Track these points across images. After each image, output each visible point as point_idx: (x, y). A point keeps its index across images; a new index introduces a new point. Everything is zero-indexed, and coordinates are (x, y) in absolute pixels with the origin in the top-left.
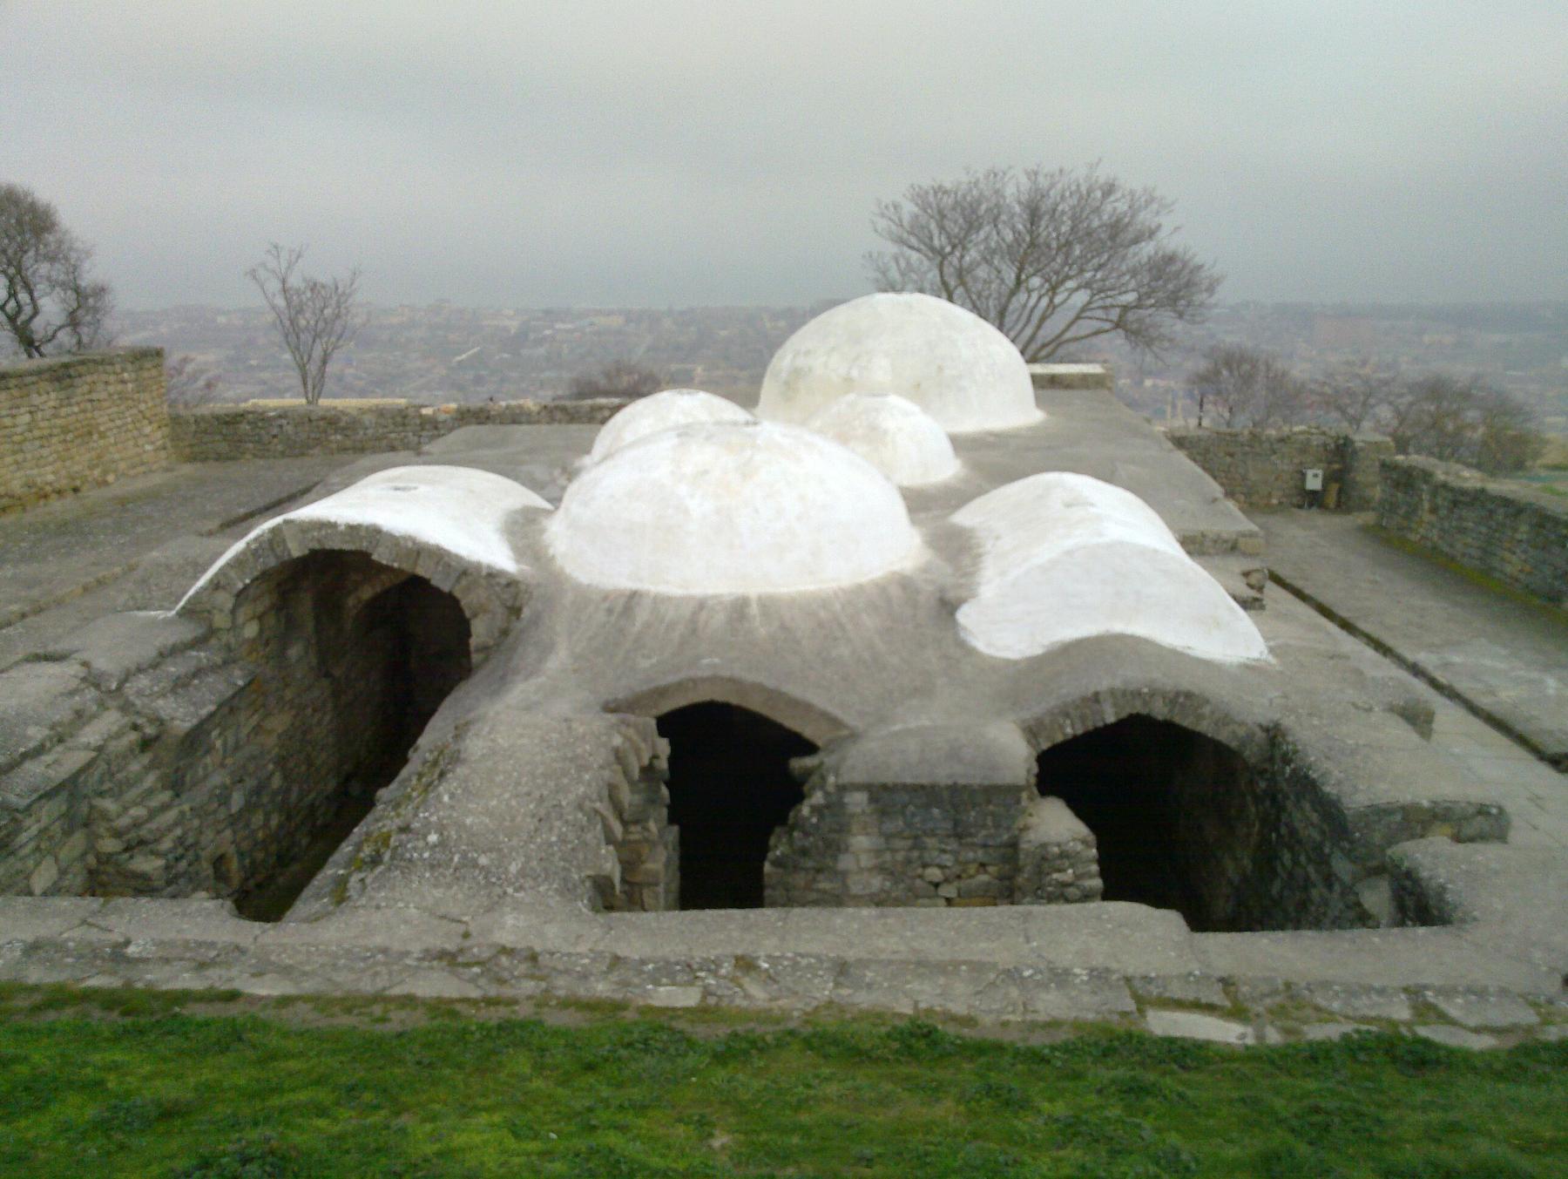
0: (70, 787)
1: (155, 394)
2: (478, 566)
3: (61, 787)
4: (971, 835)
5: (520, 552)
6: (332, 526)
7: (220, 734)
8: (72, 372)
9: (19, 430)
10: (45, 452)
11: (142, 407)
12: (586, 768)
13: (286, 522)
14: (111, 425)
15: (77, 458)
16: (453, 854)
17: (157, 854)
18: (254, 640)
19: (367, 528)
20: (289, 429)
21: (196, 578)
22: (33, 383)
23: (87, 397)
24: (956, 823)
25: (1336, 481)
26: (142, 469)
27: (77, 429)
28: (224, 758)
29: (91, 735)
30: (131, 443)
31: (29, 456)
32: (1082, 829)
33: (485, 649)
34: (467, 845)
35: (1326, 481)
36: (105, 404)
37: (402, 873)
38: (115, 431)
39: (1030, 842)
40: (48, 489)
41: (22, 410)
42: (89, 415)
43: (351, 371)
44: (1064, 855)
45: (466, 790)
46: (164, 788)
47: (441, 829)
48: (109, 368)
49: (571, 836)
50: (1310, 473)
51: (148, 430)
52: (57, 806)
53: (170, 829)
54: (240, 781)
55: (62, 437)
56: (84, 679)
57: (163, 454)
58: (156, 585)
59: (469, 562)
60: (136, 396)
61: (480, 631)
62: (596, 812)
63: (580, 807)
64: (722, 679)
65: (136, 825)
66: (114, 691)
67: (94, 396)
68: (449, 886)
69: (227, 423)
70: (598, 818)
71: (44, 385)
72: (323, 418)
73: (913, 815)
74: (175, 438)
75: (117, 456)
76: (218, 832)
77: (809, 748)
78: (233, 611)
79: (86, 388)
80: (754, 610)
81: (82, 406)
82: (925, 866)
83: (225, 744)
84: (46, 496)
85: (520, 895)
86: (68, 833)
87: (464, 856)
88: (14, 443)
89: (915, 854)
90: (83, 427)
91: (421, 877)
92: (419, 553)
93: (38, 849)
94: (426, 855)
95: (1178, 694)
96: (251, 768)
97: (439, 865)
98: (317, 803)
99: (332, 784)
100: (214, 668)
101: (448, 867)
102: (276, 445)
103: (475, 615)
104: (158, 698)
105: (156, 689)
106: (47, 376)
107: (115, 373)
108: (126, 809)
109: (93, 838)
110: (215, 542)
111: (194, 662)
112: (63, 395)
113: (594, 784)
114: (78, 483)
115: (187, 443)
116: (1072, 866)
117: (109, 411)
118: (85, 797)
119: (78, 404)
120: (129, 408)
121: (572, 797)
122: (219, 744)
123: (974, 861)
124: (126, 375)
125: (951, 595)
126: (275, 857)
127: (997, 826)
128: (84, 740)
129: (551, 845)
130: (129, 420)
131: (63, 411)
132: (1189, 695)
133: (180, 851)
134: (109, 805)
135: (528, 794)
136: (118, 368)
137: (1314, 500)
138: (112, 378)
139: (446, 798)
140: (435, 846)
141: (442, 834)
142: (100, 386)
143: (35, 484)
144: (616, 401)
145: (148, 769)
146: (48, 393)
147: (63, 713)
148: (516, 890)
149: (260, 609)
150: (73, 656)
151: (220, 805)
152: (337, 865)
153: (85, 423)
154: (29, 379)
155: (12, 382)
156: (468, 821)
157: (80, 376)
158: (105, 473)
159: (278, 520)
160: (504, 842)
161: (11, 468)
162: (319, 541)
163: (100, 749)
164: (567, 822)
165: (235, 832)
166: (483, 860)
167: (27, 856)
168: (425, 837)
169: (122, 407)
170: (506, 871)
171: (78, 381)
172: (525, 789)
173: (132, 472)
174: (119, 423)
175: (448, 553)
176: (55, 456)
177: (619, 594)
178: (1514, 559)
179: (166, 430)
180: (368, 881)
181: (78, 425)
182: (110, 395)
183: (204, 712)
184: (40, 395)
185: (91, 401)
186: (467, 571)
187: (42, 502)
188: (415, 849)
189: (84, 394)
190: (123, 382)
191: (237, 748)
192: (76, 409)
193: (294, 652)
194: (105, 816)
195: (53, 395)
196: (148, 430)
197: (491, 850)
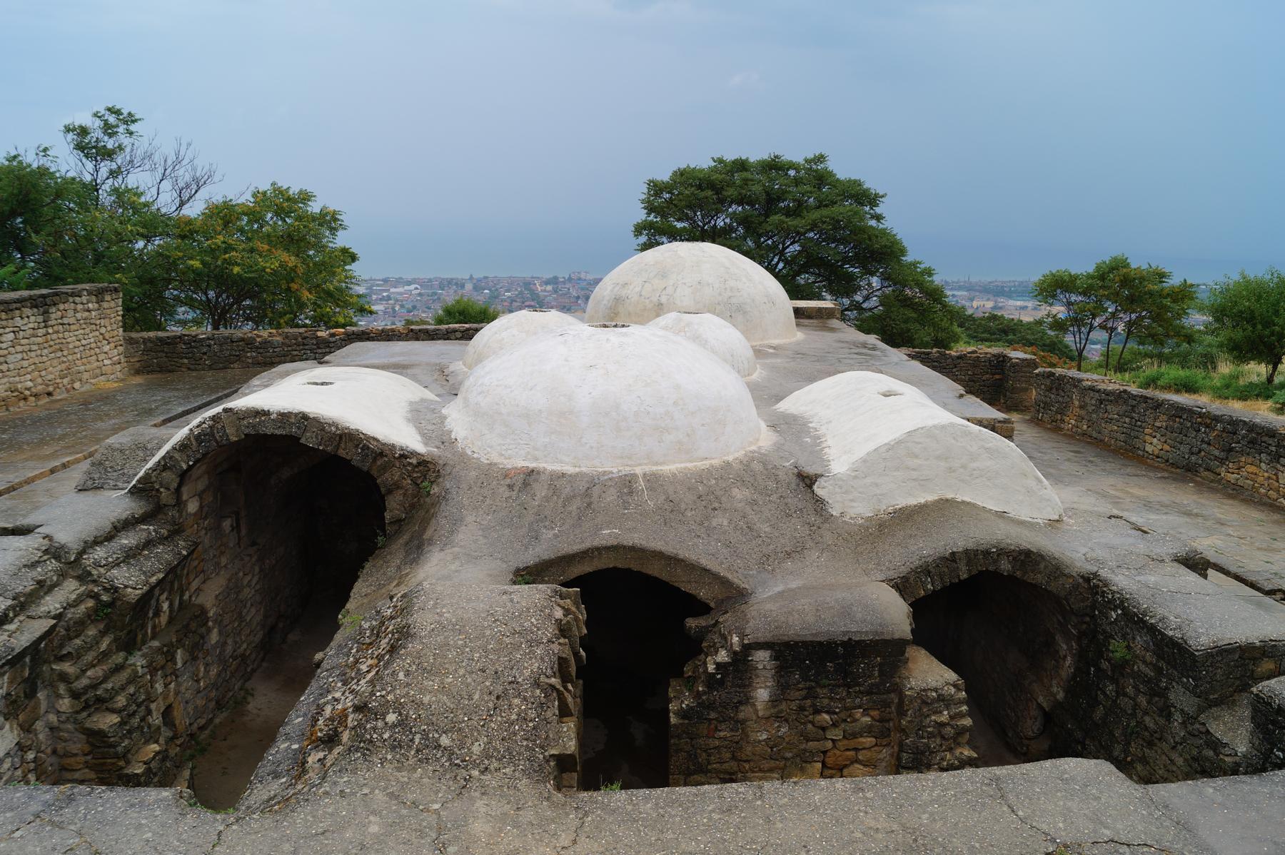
5: (426, 439)
6: (266, 413)
10: (25, 363)
11: (103, 330)
13: (225, 410)
15: (51, 368)
17: (113, 711)
18: (195, 514)
19: (296, 415)
21: (145, 461)
23: (60, 321)
27: (51, 346)
29: (52, 603)
31: (12, 366)
32: (951, 676)
33: (399, 521)
34: (428, 725)
36: (73, 327)
37: (364, 755)
38: (82, 348)
39: (911, 689)
40: (27, 393)
41: (7, 330)
42: (61, 335)
44: (941, 698)
46: (119, 650)
47: (398, 708)
48: (77, 299)
49: (532, 713)
51: (106, 348)
53: (123, 688)
55: (39, 352)
56: (46, 552)
58: (111, 467)
59: (384, 444)
60: (98, 322)
61: (394, 506)
62: (553, 687)
63: (537, 684)
64: (624, 547)
65: (94, 686)
66: (72, 562)
71: (27, 311)
75: (82, 368)
77: (702, 608)
82: (817, 711)
85: (487, 777)
87: (425, 735)
89: (808, 702)
90: (55, 344)
91: (383, 761)
92: (341, 436)
94: (386, 736)
97: (401, 747)
98: (248, 652)
99: (260, 635)
100: (163, 540)
102: (205, 360)
103: (390, 492)
104: (113, 567)
105: (110, 560)
107: (82, 304)
108: (84, 671)
110: (163, 431)
111: (144, 535)
113: (546, 659)
114: (51, 389)
115: (136, 359)
116: (947, 707)
117: (76, 333)
120: (92, 331)
121: (527, 673)
125: (810, 470)
126: (214, 703)
128: (43, 609)
130: (92, 340)
132: (1028, 553)
133: (134, 707)
134: (67, 667)
136: (84, 299)
138: (80, 307)
140: (394, 726)
141: (400, 714)
142: (71, 313)
143: (16, 390)
144: (475, 326)
145: (103, 634)
146: (28, 317)
147: (25, 584)
148: (482, 773)
150: (36, 531)
151: (167, 661)
152: (288, 737)
153: (58, 341)
154: (14, 306)
156: (426, 700)
157: (55, 304)
158: (73, 381)
159: (218, 409)
160: (464, 721)
162: (254, 426)
163: (59, 617)
164: (525, 699)
166: (445, 741)
168: (384, 715)
169: (87, 331)
170: (470, 753)
174: (84, 342)
176: (33, 367)
177: (518, 471)
178: (1155, 441)
179: (121, 349)
180: (328, 763)
181: (52, 343)
183: (153, 580)
184: (22, 318)
188: (374, 729)
189: (56, 319)
190: (89, 311)
195: (32, 319)
196: (106, 348)
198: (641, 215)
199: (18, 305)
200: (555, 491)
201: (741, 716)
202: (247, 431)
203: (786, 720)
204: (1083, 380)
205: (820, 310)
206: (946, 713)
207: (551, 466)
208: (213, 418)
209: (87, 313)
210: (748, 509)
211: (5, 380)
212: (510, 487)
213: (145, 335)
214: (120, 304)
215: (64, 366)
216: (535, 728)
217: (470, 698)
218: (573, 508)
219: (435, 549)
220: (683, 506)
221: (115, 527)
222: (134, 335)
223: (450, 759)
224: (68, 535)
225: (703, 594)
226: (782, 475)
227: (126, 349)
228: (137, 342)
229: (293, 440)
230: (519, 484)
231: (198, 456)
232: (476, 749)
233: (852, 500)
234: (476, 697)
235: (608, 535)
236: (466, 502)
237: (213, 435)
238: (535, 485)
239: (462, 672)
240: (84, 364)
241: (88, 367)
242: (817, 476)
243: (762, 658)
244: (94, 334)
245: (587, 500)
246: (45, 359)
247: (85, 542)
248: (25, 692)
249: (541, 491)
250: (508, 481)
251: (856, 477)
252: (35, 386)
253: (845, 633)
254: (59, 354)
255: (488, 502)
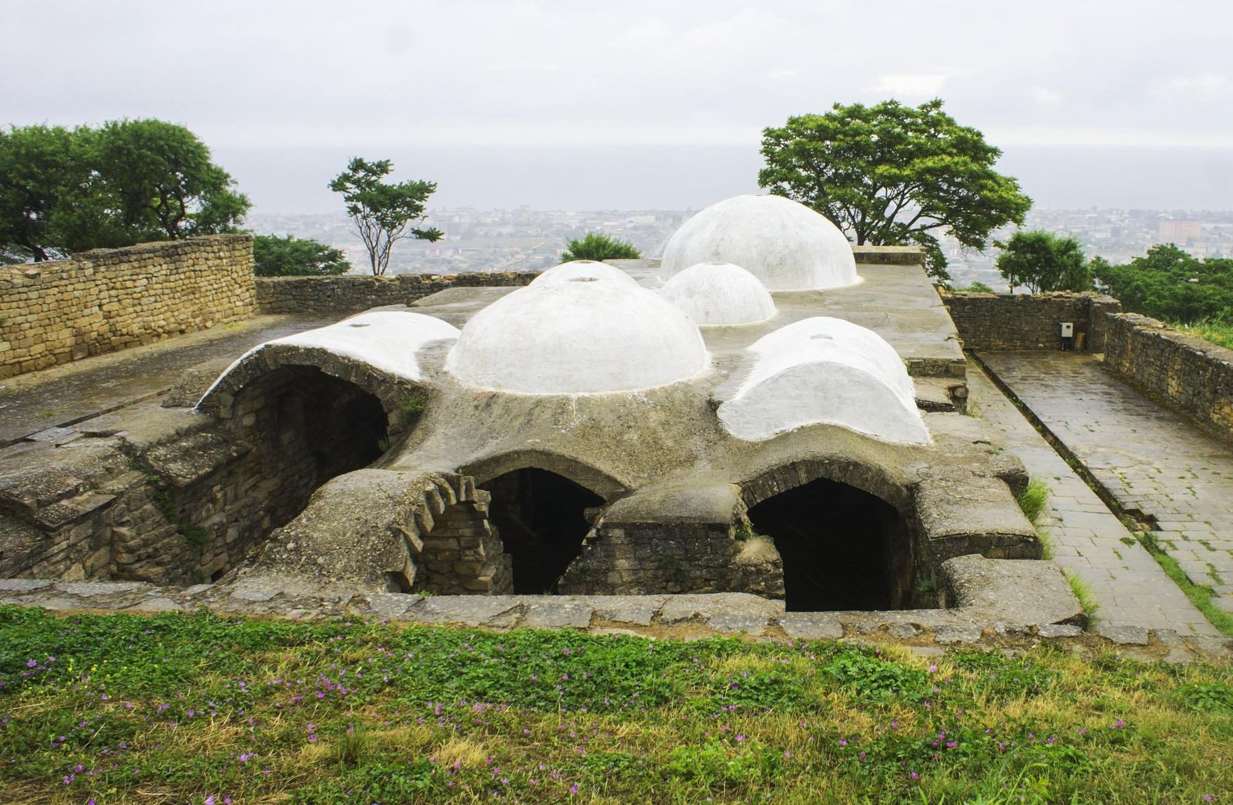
0: (96, 516)
1: (244, 267)
2: (392, 377)
3: (86, 516)
4: (698, 560)
5: (424, 368)
6: (296, 349)
7: (221, 490)
8: (180, 251)
9: (137, 290)
10: (158, 305)
11: (235, 275)
12: (400, 503)
14: (210, 287)
16: (302, 556)
18: (251, 427)
19: (318, 350)
20: (339, 291)
22: (149, 258)
24: (687, 551)
25: (1083, 331)
26: (233, 318)
27: (183, 290)
28: (225, 505)
30: (226, 300)
31: (145, 308)
35: (1075, 331)
36: (204, 274)
38: (213, 292)
40: (160, 330)
41: (141, 276)
42: (193, 281)
43: (458, 257)
44: (759, 572)
45: (318, 516)
48: (209, 249)
49: (380, 546)
50: (1064, 325)
51: (238, 291)
52: (87, 529)
54: (236, 521)
55: (171, 295)
56: (120, 449)
57: (250, 308)
60: (229, 268)
64: (536, 452)
67: (197, 268)
68: (296, 576)
69: (295, 287)
70: (402, 536)
72: (363, 284)
73: (657, 545)
74: (259, 297)
75: (214, 309)
76: (216, 555)
78: (233, 406)
79: (191, 262)
80: (573, 406)
81: (188, 274)
83: (225, 495)
84: (159, 336)
86: (94, 548)
87: (309, 558)
88: (134, 299)
93: (67, 558)
95: (849, 464)
96: (245, 512)
97: (292, 563)
100: (218, 444)
101: (298, 564)
103: (391, 411)
106: (160, 253)
107: (214, 252)
109: (114, 552)
112: (172, 266)
114: (183, 327)
118: (109, 525)
119: (184, 273)
121: (386, 521)
122: (219, 495)
123: (701, 577)
124: (222, 254)
125: (716, 398)
127: (714, 552)
129: (366, 552)
130: (224, 284)
131: (172, 278)
135: (358, 519)
136: (216, 249)
137: (1067, 346)
138: (211, 255)
139: (304, 521)
140: (291, 550)
142: (202, 261)
143: (150, 328)
146: (160, 265)
148: (338, 580)
149: (257, 405)
154: (147, 256)
155: (133, 257)
156: (315, 535)
158: (205, 321)
161: (132, 316)
164: (379, 537)
165: (230, 556)
166: (321, 560)
167: (58, 562)
169: (219, 276)
170: (334, 568)
171: (184, 257)
172: (357, 516)
173: (225, 320)
174: (215, 286)
175: (372, 368)
179: (253, 292)
181: (184, 287)
182: (209, 267)
185: (194, 271)
186: (387, 380)
187: (155, 339)
188: (278, 552)
190: (220, 258)
191: (236, 498)
192: (182, 276)
193: (286, 437)
194: (122, 538)
195: (165, 266)
196: (238, 291)
197: (326, 554)
198: (763, 163)
199: (151, 255)
200: (507, 411)
201: (610, 580)
202: (282, 362)
203: (645, 585)
204: (1135, 325)
205: (905, 255)
206: (763, 584)
207: (508, 392)
208: (258, 352)
209: (218, 261)
210: (660, 429)
211: (140, 319)
212: (476, 407)
213: (276, 279)
214: (252, 252)
215: (196, 307)
216: (380, 555)
217: (344, 535)
218: (516, 423)
219: (406, 452)
220: (603, 423)
221: (178, 433)
222: (266, 280)
223: (320, 571)
224: (137, 438)
225: (598, 489)
226: (697, 402)
227: (258, 293)
228: (268, 286)
229: (316, 369)
230: (483, 405)
231: (247, 381)
232: (338, 566)
233: (746, 423)
234: (348, 535)
235: (532, 441)
236: (441, 418)
237: (258, 365)
238: (493, 406)
239: (344, 519)
240: (215, 306)
241: (220, 308)
242: (720, 403)
243: (618, 534)
244: (226, 279)
245: (528, 418)
246: (177, 301)
247: (151, 443)
248: (90, 546)
249: (497, 410)
250: (476, 402)
251: (747, 404)
252: (168, 324)
253: (678, 518)
254: (191, 297)
255: (458, 418)
